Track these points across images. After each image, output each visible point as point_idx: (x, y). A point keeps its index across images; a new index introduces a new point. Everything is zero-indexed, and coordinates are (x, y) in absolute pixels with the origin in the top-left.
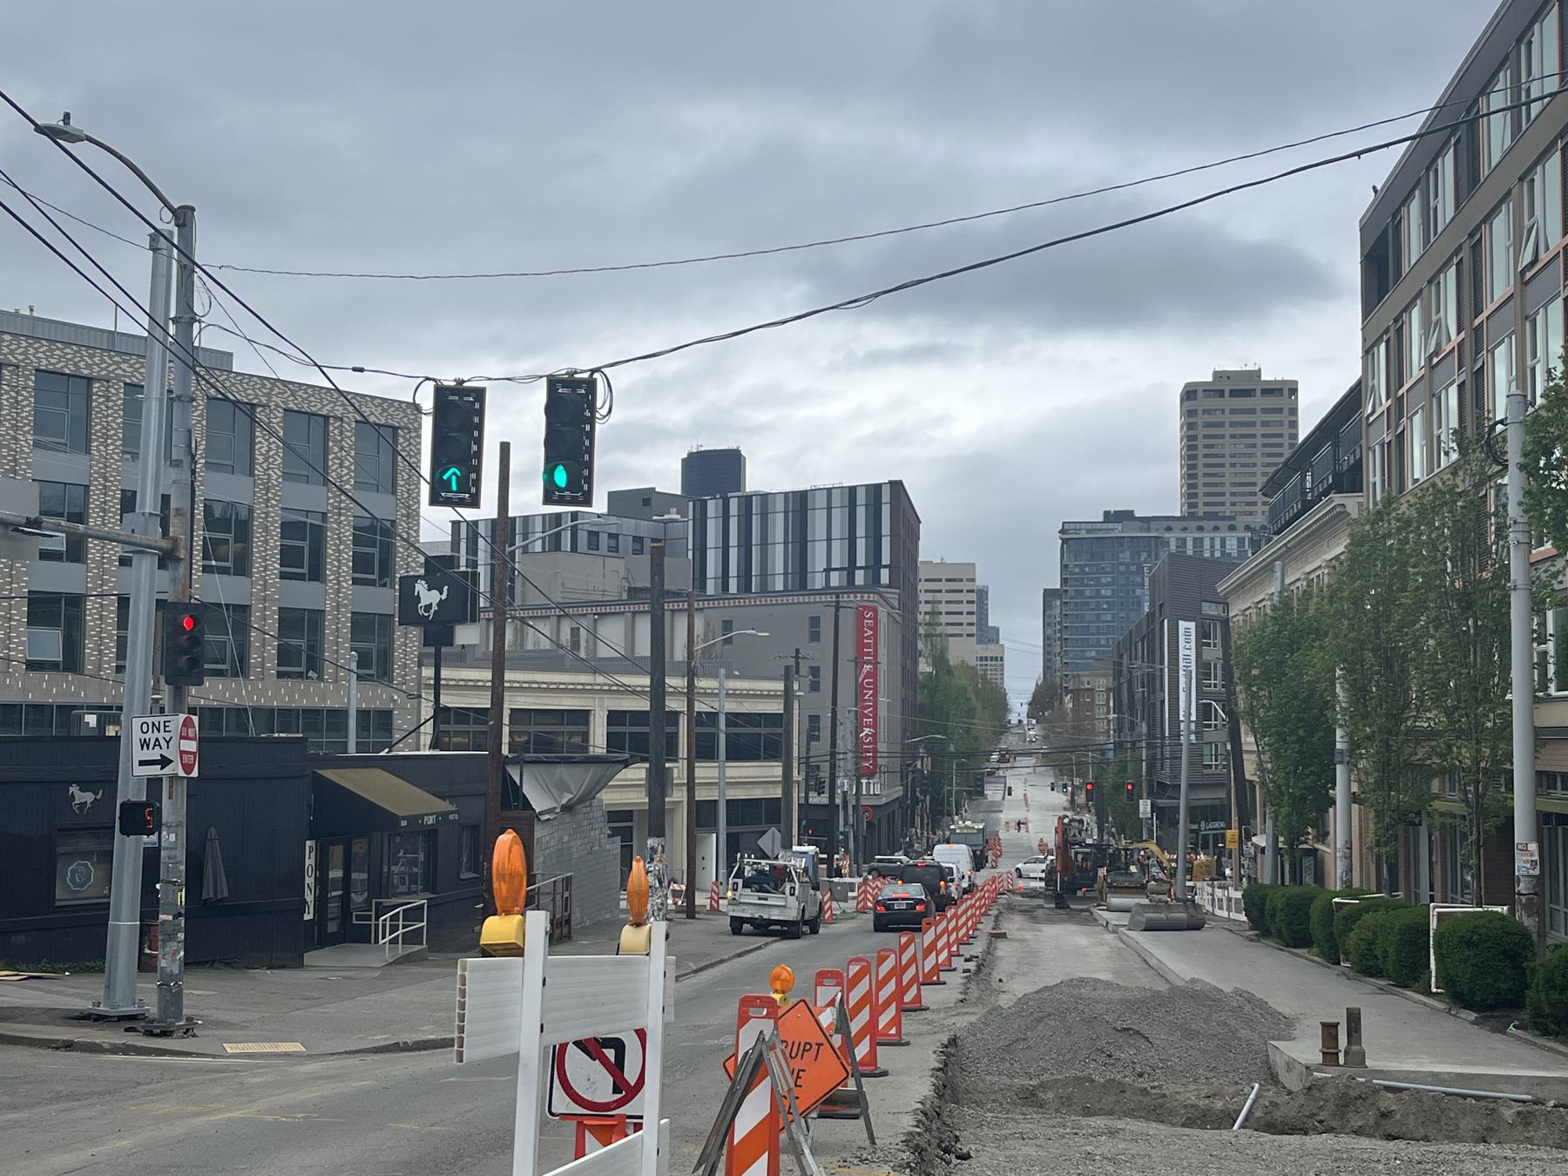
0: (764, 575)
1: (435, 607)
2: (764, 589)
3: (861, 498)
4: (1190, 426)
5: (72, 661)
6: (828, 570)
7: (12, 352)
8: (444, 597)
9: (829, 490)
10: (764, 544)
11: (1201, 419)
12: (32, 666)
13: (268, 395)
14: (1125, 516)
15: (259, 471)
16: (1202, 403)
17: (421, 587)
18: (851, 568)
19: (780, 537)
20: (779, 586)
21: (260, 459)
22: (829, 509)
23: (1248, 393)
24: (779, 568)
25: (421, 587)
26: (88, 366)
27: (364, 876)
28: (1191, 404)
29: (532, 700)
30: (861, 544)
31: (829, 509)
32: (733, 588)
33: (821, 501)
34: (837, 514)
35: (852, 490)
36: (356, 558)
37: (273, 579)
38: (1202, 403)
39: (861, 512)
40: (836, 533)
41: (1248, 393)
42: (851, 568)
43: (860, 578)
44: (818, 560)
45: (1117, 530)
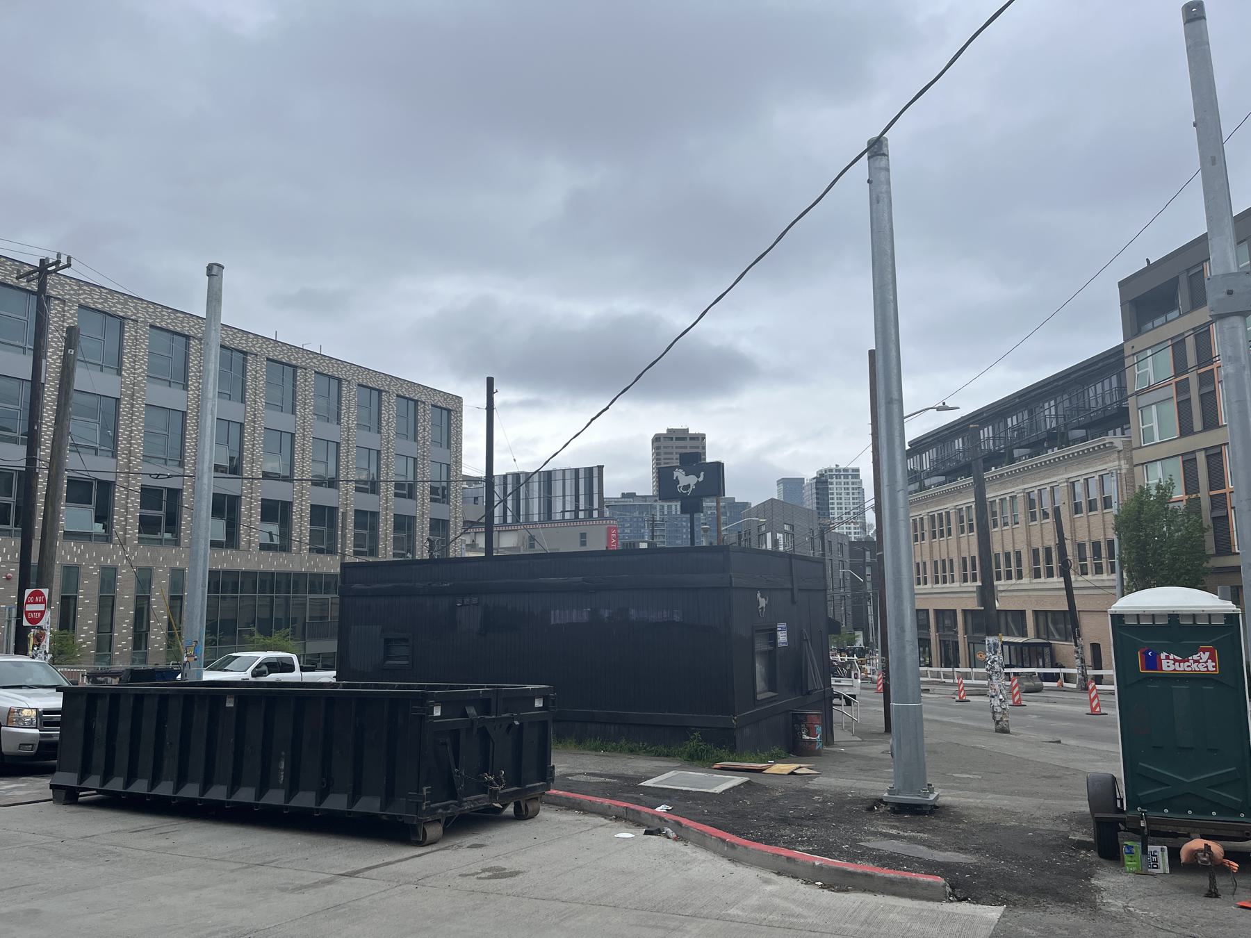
0: (527, 514)
1: (692, 487)
2: (527, 522)
3: (582, 475)
4: (658, 454)
5: (285, 547)
6: (564, 512)
7: (254, 346)
8: (701, 479)
9: (564, 471)
10: (527, 499)
11: (662, 450)
12: (263, 547)
13: (389, 385)
14: (632, 495)
15: (384, 430)
16: (663, 443)
17: (679, 474)
18: (577, 510)
19: (536, 494)
20: (536, 518)
21: (384, 423)
22: (564, 480)
23: (683, 439)
24: (536, 511)
25: (679, 474)
26: (296, 359)
27: (228, 705)
28: (656, 444)
29: (198, 611)
30: (582, 498)
31: (564, 480)
32: (509, 520)
33: (559, 476)
34: (568, 483)
35: (577, 470)
36: (142, 519)
37: (391, 496)
38: (663, 443)
39: (582, 482)
40: (568, 493)
41: (683, 439)
42: (577, 510)
43: (581, 515)
44: (558, 506)
45: (630, 502)
